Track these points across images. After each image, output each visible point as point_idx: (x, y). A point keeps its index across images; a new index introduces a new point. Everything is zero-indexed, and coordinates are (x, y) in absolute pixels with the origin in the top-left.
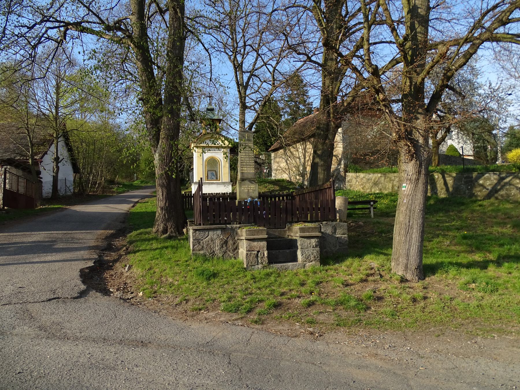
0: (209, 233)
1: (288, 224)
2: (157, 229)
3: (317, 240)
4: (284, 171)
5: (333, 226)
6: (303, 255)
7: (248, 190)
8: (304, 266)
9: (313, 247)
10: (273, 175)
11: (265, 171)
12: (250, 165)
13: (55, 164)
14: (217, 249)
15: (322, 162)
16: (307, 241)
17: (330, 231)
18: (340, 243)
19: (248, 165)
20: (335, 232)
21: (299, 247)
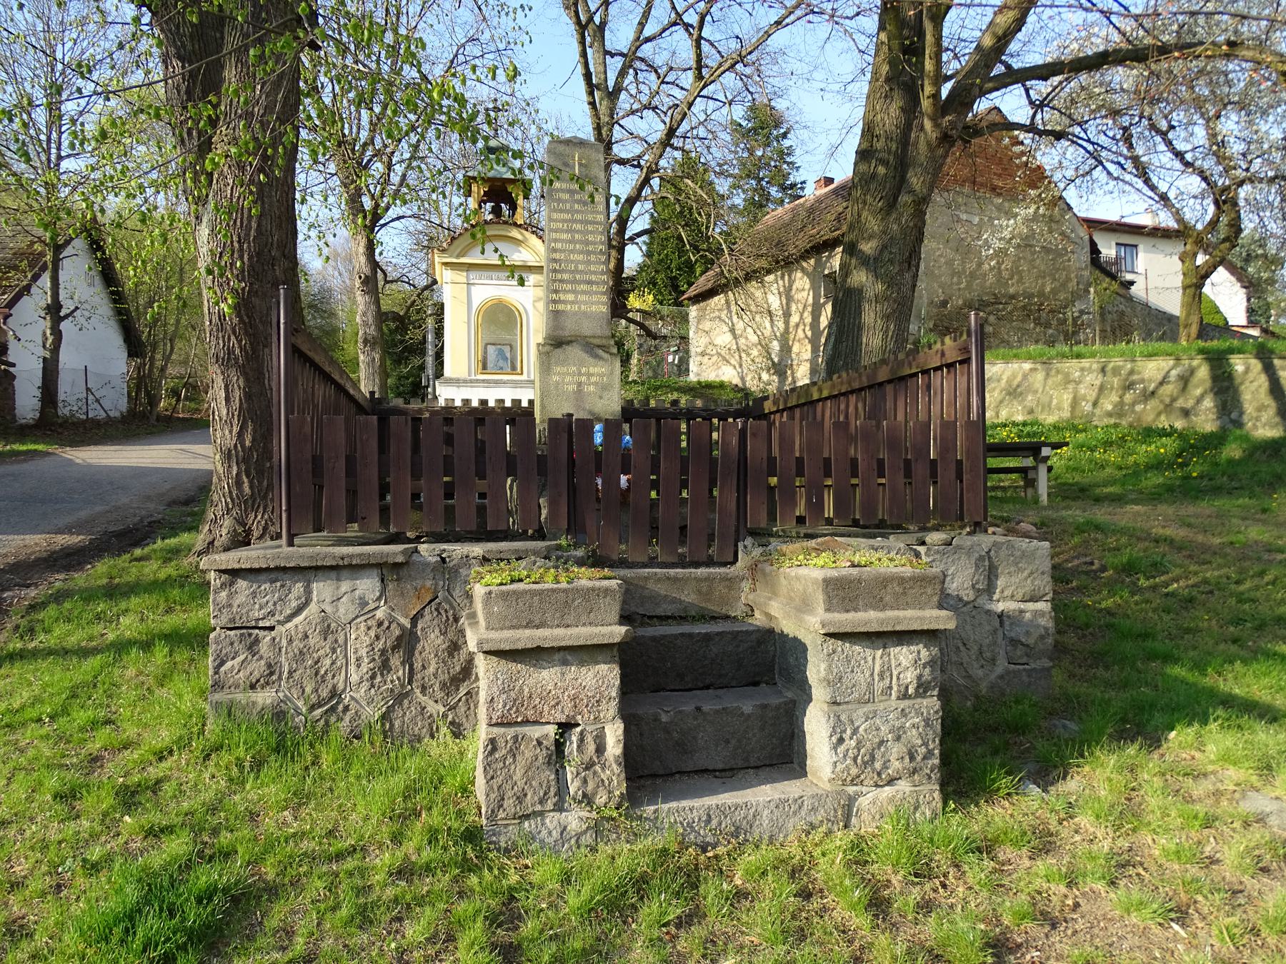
0: (308, 592)
1: (749, 541)
2: (210, 539)
3: (925, 654)
4: (724, 359)
5: (981, 558)
6: (841, 740)
7: (580, 384)
8: (848, 812)
9: (904, 696)
10: (693, 367)
11: (670, 359)
12: (590, 283)
13: (49, 324)
14: (354, 678)
15: (880, 287)
16: (872, 658)
17: (968, 584)
18: (1014, 642)
19: (580, 282)
20: (990, 590)
21: (819, 694)
